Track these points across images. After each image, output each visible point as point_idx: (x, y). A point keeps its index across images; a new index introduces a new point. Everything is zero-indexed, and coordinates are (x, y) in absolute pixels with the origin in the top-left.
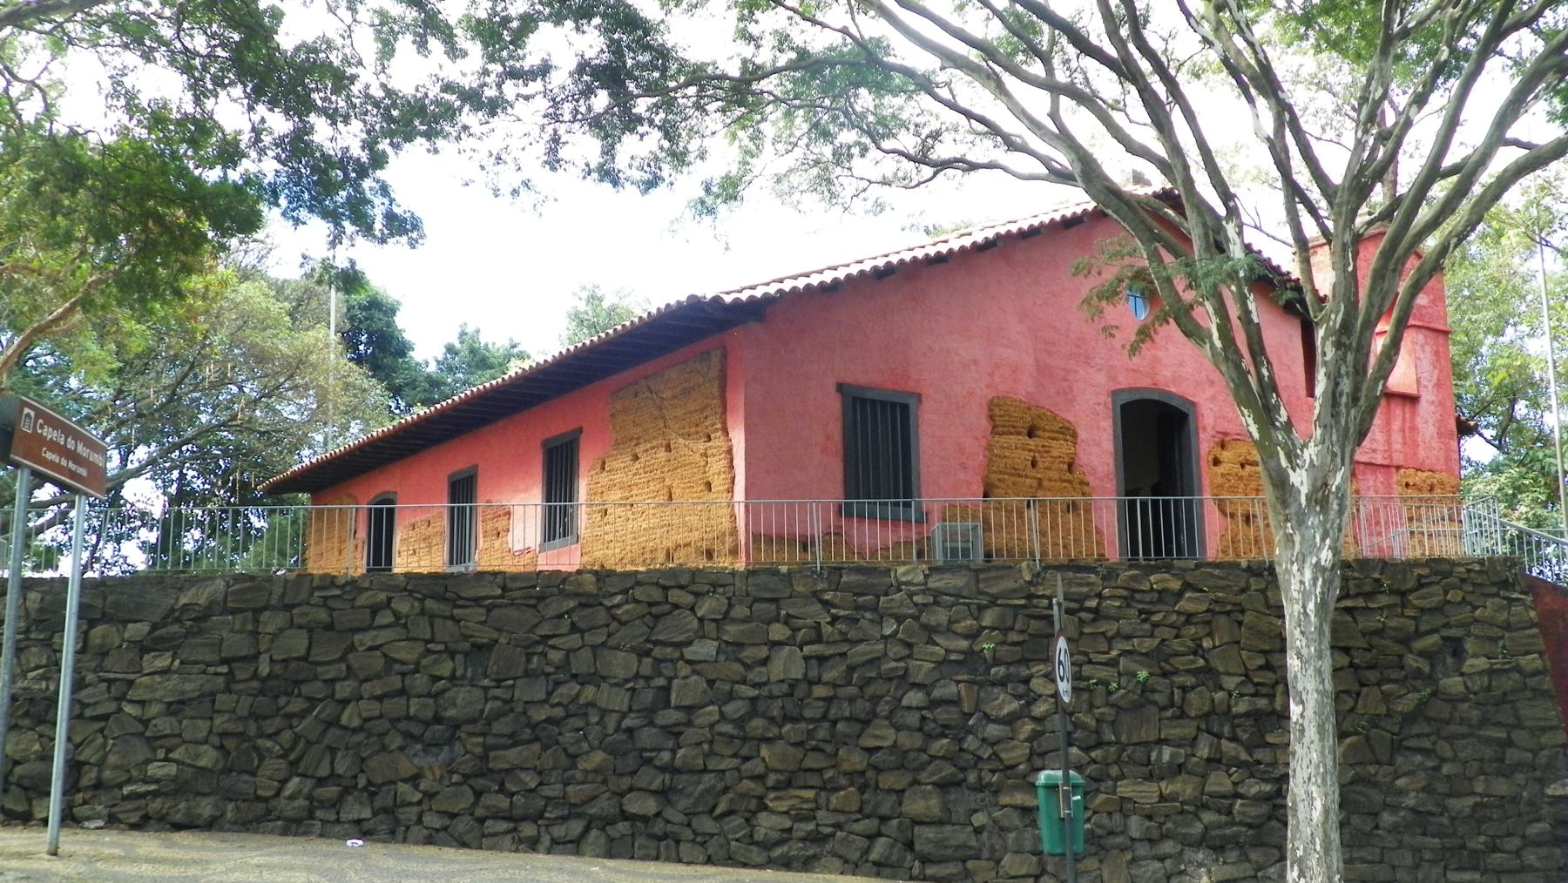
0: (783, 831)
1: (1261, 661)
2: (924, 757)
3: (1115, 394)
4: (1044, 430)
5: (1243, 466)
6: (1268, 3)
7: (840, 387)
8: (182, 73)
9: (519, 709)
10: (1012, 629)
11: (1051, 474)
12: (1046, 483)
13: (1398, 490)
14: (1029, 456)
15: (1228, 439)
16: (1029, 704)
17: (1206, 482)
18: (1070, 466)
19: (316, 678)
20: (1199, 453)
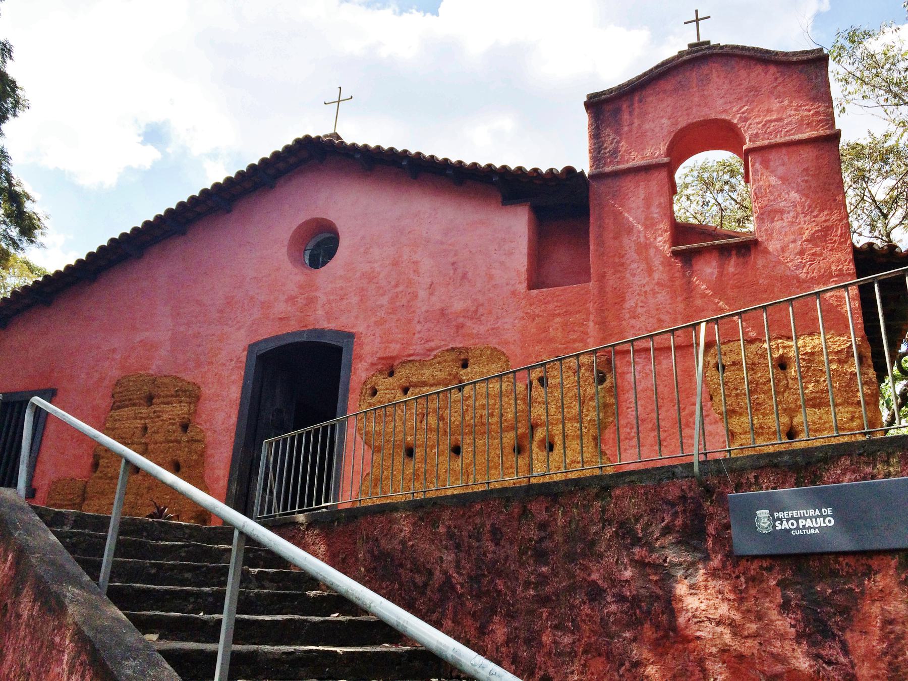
7: (438, 15)
14: (139, 423)
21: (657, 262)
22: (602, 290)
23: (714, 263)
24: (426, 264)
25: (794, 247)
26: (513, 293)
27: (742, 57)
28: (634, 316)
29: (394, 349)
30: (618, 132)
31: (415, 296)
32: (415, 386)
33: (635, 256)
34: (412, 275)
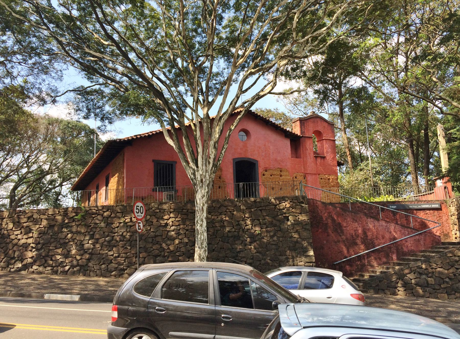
0: (115, 268)
1: (237, 223)
2: (152, 249)
3: (234, 159)
5: (271, 176)
8: (449, 165)
9: (58, 240)
10: (177, 217)
13: (319, 180)
16: (178, 235)
18: (220, 178)
19: (13, 234)
24: (271, 147)
25: (330, 159)
26: (289, 158)
29: (267, 166)
31: (270, 154)
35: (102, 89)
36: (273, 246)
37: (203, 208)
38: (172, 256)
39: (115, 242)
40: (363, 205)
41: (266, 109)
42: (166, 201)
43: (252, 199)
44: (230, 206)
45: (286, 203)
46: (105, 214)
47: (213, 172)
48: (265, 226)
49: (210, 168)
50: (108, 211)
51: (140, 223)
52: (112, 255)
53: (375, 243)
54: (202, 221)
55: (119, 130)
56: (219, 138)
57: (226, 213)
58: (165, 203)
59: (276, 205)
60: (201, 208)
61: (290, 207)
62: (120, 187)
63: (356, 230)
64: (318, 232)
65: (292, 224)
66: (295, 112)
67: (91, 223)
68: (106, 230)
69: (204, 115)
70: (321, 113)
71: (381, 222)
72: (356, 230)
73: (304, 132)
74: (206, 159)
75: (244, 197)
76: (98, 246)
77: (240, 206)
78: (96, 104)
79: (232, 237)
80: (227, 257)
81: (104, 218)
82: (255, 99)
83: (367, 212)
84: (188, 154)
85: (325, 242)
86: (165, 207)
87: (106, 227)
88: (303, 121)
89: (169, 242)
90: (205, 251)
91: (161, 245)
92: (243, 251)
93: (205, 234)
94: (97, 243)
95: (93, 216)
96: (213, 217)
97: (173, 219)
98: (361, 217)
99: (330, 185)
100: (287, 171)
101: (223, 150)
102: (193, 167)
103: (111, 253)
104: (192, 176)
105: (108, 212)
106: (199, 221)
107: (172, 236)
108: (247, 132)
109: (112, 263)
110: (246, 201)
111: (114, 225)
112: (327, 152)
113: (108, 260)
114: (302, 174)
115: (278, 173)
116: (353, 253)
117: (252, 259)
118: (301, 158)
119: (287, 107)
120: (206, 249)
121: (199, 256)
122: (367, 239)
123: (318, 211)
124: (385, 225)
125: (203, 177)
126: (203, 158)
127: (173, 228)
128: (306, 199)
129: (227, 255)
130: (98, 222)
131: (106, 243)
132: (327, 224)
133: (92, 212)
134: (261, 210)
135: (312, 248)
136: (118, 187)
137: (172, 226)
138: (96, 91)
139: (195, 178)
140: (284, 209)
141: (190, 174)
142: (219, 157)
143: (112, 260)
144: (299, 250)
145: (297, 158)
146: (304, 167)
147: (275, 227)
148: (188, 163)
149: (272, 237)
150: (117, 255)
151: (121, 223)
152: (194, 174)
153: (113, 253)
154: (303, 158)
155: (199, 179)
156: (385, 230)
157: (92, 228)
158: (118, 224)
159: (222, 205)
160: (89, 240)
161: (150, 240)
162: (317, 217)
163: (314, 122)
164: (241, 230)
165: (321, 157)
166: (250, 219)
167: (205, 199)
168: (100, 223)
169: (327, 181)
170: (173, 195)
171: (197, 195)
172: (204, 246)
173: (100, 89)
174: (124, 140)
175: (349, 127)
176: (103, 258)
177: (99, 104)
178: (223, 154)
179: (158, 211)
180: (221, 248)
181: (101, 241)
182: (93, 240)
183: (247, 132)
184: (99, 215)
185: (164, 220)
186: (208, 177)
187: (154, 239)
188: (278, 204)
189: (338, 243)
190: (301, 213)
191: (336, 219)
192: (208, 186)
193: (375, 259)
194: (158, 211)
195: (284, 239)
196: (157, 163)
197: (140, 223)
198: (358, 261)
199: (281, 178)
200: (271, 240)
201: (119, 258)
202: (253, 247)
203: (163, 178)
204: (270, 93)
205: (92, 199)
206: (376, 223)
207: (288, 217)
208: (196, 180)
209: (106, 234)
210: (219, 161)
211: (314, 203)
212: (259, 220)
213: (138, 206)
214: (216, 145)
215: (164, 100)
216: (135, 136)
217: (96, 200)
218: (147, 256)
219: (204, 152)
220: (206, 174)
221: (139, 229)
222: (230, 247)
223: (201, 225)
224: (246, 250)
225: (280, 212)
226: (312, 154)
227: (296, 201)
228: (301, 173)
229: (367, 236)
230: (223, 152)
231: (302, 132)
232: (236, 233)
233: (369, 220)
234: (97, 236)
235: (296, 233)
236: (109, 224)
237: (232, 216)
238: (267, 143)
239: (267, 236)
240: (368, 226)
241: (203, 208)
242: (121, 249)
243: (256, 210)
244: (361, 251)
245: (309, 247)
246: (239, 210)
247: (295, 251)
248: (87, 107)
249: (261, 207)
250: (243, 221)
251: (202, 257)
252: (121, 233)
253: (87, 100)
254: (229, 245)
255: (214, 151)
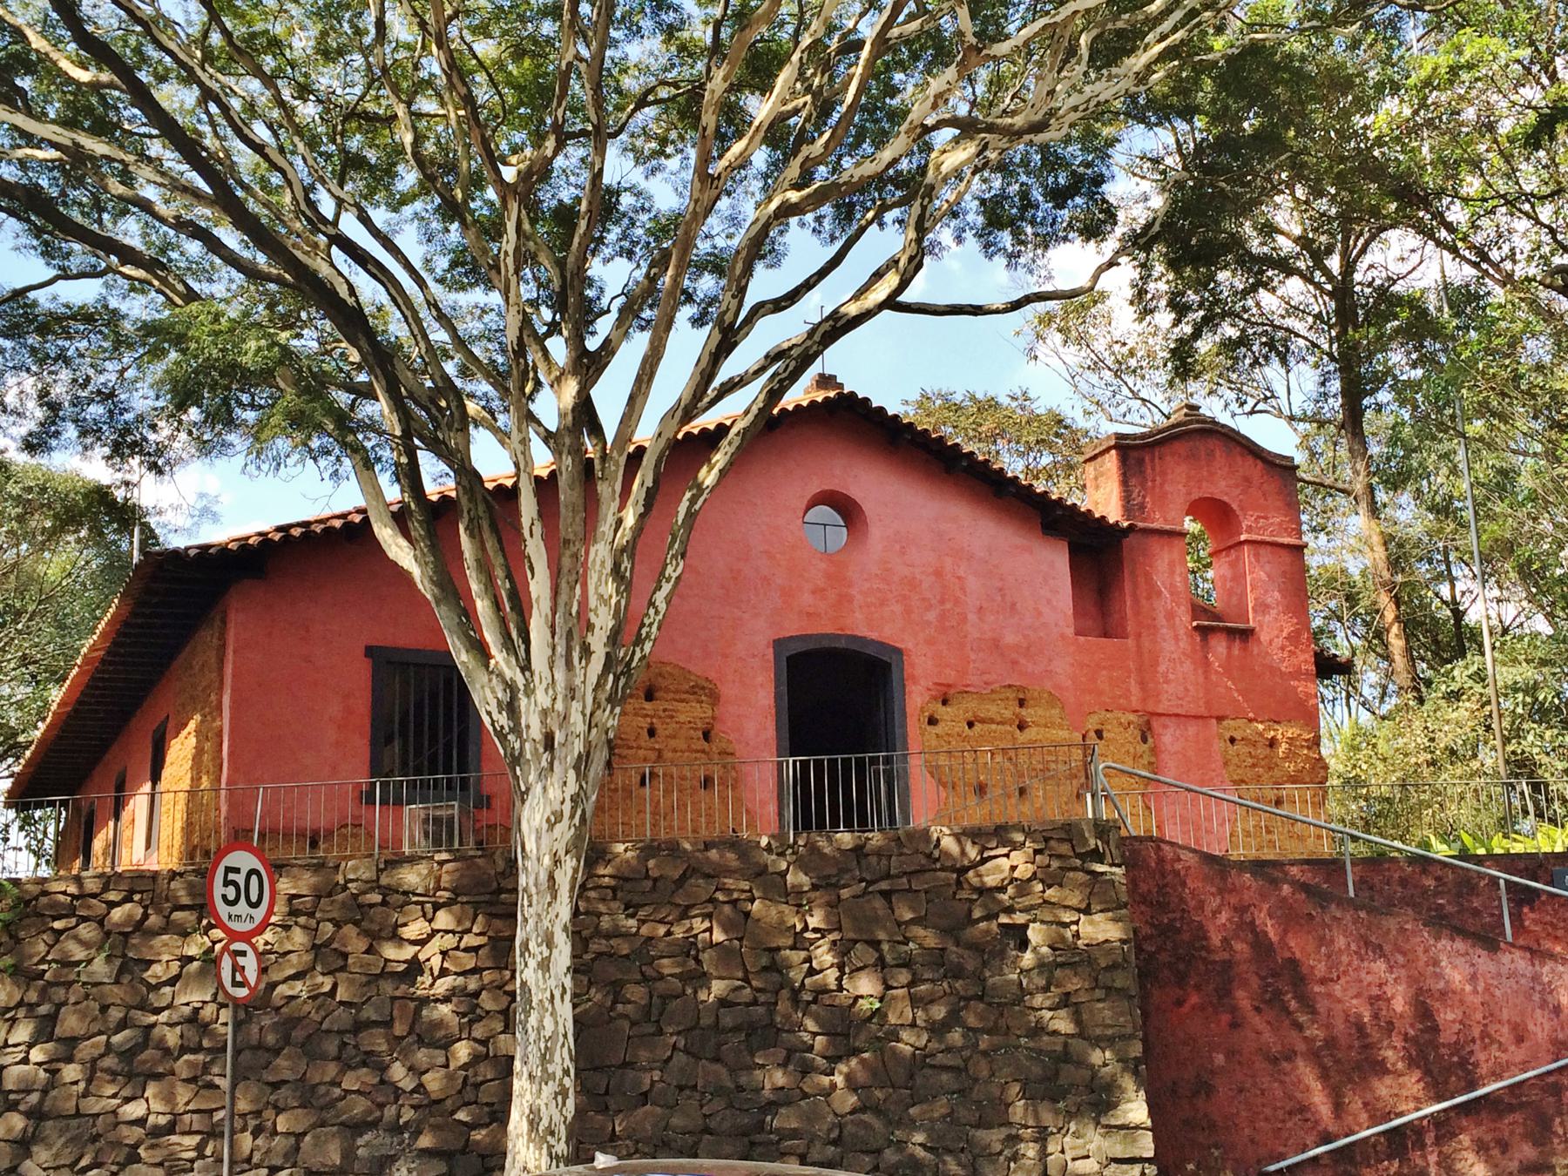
2: (337, 1092)
3: (778, 644)
4: (667, 690)
5: (970, 725)
6: (1560, 352)
7: (370, 651)
10: (469, 931)
11: (680, 744)
12: (668, 755)
13: (1219, 746)
14: (645, 723)
15: (952, 691)
16: (471, 1022)
17: (914, 747)
18: (707, 736)
20: (904, 709)
21: (1182, 632)
22: (1139, 647)
23: (1224, 644)
24: (973, 583)
25: (1279, 642)
26: (1063, 636)
27: (1239, 443)
28: (1167, 682)
29: (950, 676)
30: (1143, 484)
31: (964, 620)
32: (983, 721)
33: (1164, 622)
34: (959, 594)
35: (113, 303)
36: (945, 1077)
37: (551, 878)
38: (435, 1128)
39: (158, 1054)
40: (1424, 871)
41: (973, 398)
42: (423, 846)
43: (845, 838)
44: (730, 872)
45: (1018, 857)
46: (117, 914)
47: (609, 700)
48: (904, 977)
49: (593, 679)
50: (128, 899)
51: (243, 954)
52: (141, 1122)
53: (1476, 1065)
54: (549, 942)
55: (199, 506)
56: (639, 530)
57: (710, 908)
58: (412, 860)
59: (966, 869)
60: (543, 877)
61: (1034, 876)
62: (205, 783)
63: (1378, 998)
64: (1186, 1008)
65: (1041, 965)
66: (1123, 408)
67: (43, 961)
68: (116, 993)
69: (562, 415)
70: (1252, 412)
71: (1506, 958)
72: (1378, 1000)
73: (1142, 507)
74: (573, 635)
75: (807, 827)
76: (71, 1072)
77: (783, 874)
78: (88, 380)
79: (736, 1029)
80: (707, 1130)
81: (108, 934)
82: (817, 337)
83: (1450, 909)
84: (482, 606)
85: (1220, 1059)
86: (412, 877)
87: (117, 982)
88: (1134, 454)
89: (422, 1056)
90: (563, 1092)
91: (383, 1068)
92: (788, 1104)
93: (566, 1011)
94: (69, 1060)
95: (57, 925)
96: (644, 930)
97: (449, 941)
98: (1402, 930)
99: (1277, 773)
100: (1053, 700)
101: (659, 588)
102: (508, 674)
103: (135, 1110)
104: (503, 720)
105: (128, 906)
106: (532, 945)
107: (440, 1024)
108: (848, 510)
109: (138, 1159)
110: (812, 848)
111: (157, 969)
112: (1262, 607)
113: (118, 1144)
114: (1132, 717)
115: (1008, 714)
116: (1364, 1116)
117: (835, 1143)
118: (1124, 636)
119: (1083, 387)
120: (568, 1082)
121: (531, 1123)
122: (1436, 1047)
123: (1182, 900)
124: (1529, 971)
125: (553, 723)
126: (553, 627)
127: (443, 986)
128: (1113, 837)
129: (713, 1124)
130: (79, 953)
131: (110, 1062)
132: (1228, 965)
133: (57, 904)
134: (887, 895)
135: (1140, 1084)
136: (196, 780)
137: (444, 972)
138: (86, 316)
139: (516, 729)
140: (1002, 889)
141: (493, 708)
142: (642, 625)
143: (136, 1146)
144: (1071, 1099)
145: (1106, 635)
146: (1142, 684)
147: (956, 977)
148: (481, 650)
149: (937, 1029)
150: (162, 1120)
151: (191, 959)
152: (511, 708)
153: (149, 1106)
154: (1139, 635)
155: (536, 732)
156: (1529, 998)
157: (50, 984)
158: (175, 968)
159: (691, 871)
160: (31, 1046)
161: (331, 1047)
162: (1179, 931)
163: (1192, 457)
164: (785, 993)
165: (1231, 633)
166: (831, 937)
167: (564, 832)
168: (89, 961)
169: (1262, 751)
170: (451, 819)
171: (525, 814)
172: (556, 1068)
173: (103, 301)
174: (223, 550)
175: (1396, 482)
176: (95, 1138)
177: (102, 379)
178: (662, 607)
179: (376, 898)
180: (681, 1088)
181: (86, 1050)
182: (50, 1045)
183: (848, 510)
184: (85, 919)
185: (400, 941)
186: (578, 722)
187: (348, 1039)
188: (975, 865)
189: (1286, 1065)
190: (1087, 911)
191: (1272, 934)
192: (582, 764)
193: (1481, 1148)
194: (376, 898)
195: (996, 1039)
196: (384, 660)
197: (243, 954)
198: (1390, 1157)
199: (1022, 737)
200: (934, 1045)
201: (174, 1138)
202: (839, 1079)
203: (419, 734)
204: (891, 303)
205: (98, 844)
206: (1483, 961)
207: (1025, 927)
208: (519, 735)
209: (116, 1014)
210: (639, 641)
211: (1161, 860)
212: (875, 944)
213: (237, 871)
214: (626, 564)
215: (366, 347)
216: (279, 529)
217: (113, 848)
218: (314, 1126)
219: (563, 598)
220: (567, 708)
221: (235, 984)
222: (730, 1084)
223: (545, 965)
224: (805, 1096)
225: (984, 906)
226: (1186, 618)
227: (1064, 849)
228: (1124, 710)
229: (1435, 1029)
230: (660, 598)
231: (1128, 509)
232: (761, 1010)
233: (1444, 943)
234: (70, 1023)
235: (1062, 1013)
236: (130, 967)
237: (741, 922)
238: (948, 561)
239: (913, 1025)
240: (1438, 976)
241: (551, 878)
242: (183, 1094)
243: (865, 893)
244: (1403, 1107)
245: (1128, 1083)
246: (775, 887)
247: (1055, 1100)
248: (43, 395)
249: (888, 876)
250: (793, 948)
251: (545, 1123)
252: (187, 1010)
253: (42, 359)
254: (723, 1071)
255: (610, 588)
